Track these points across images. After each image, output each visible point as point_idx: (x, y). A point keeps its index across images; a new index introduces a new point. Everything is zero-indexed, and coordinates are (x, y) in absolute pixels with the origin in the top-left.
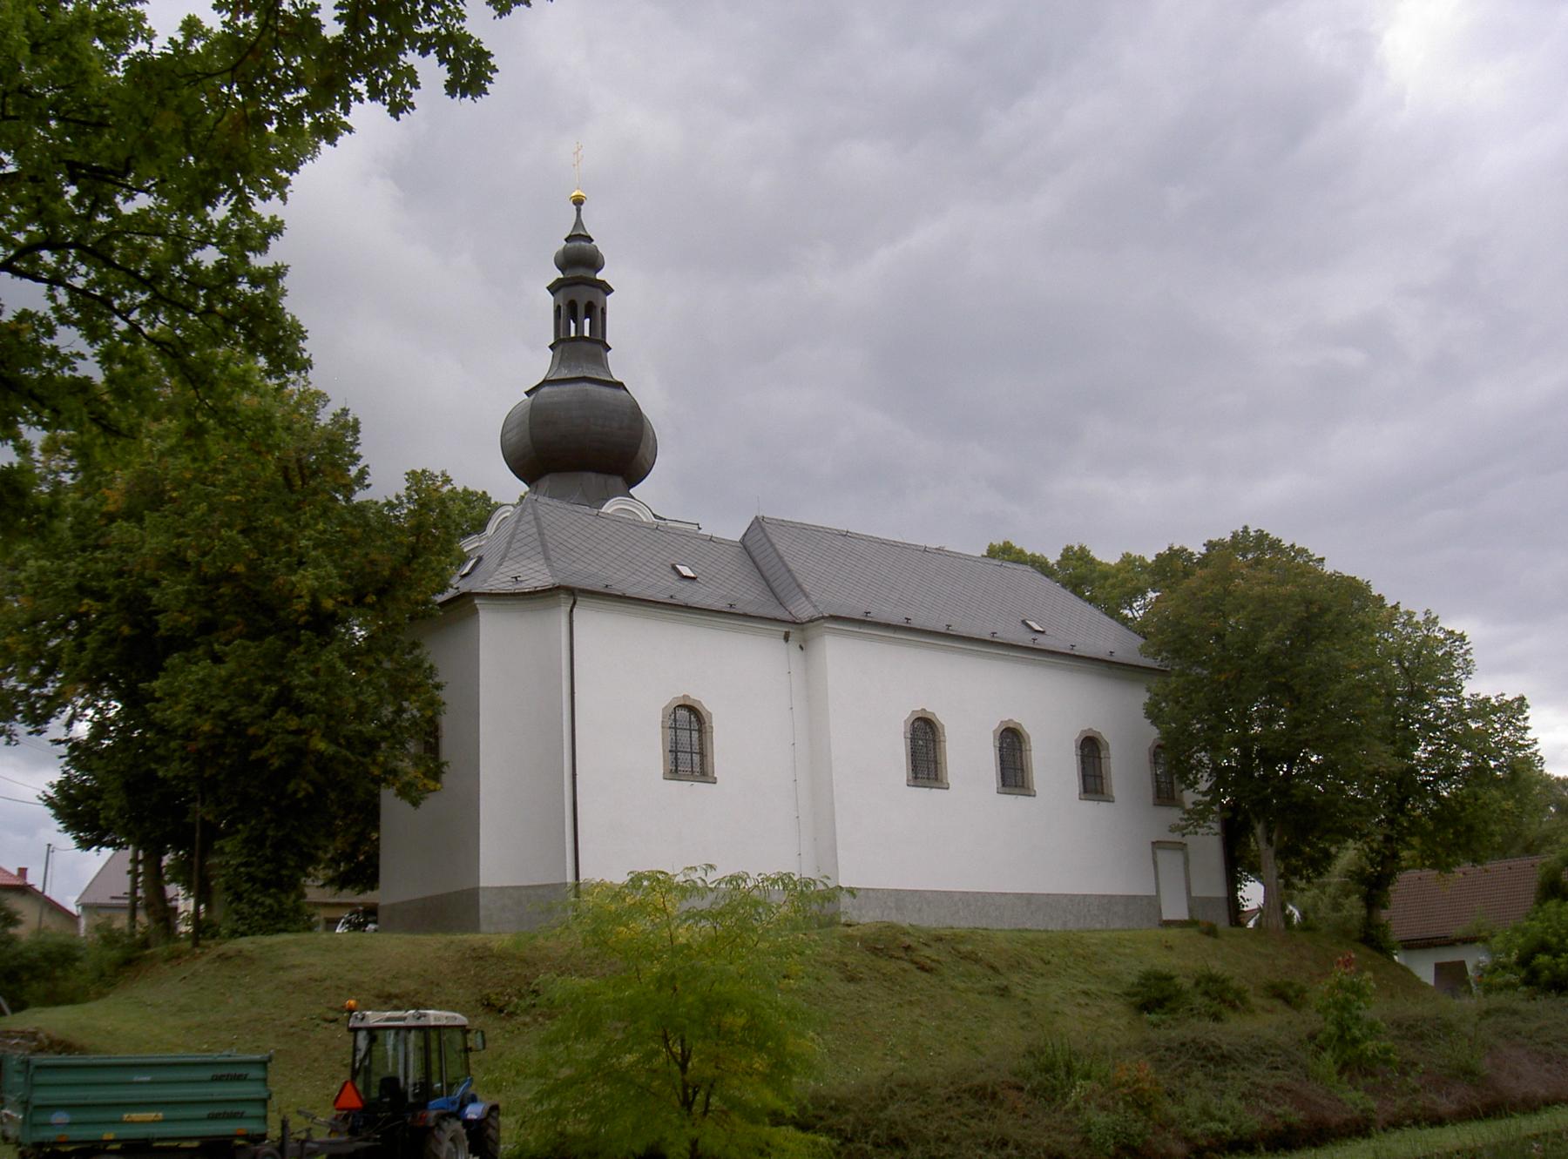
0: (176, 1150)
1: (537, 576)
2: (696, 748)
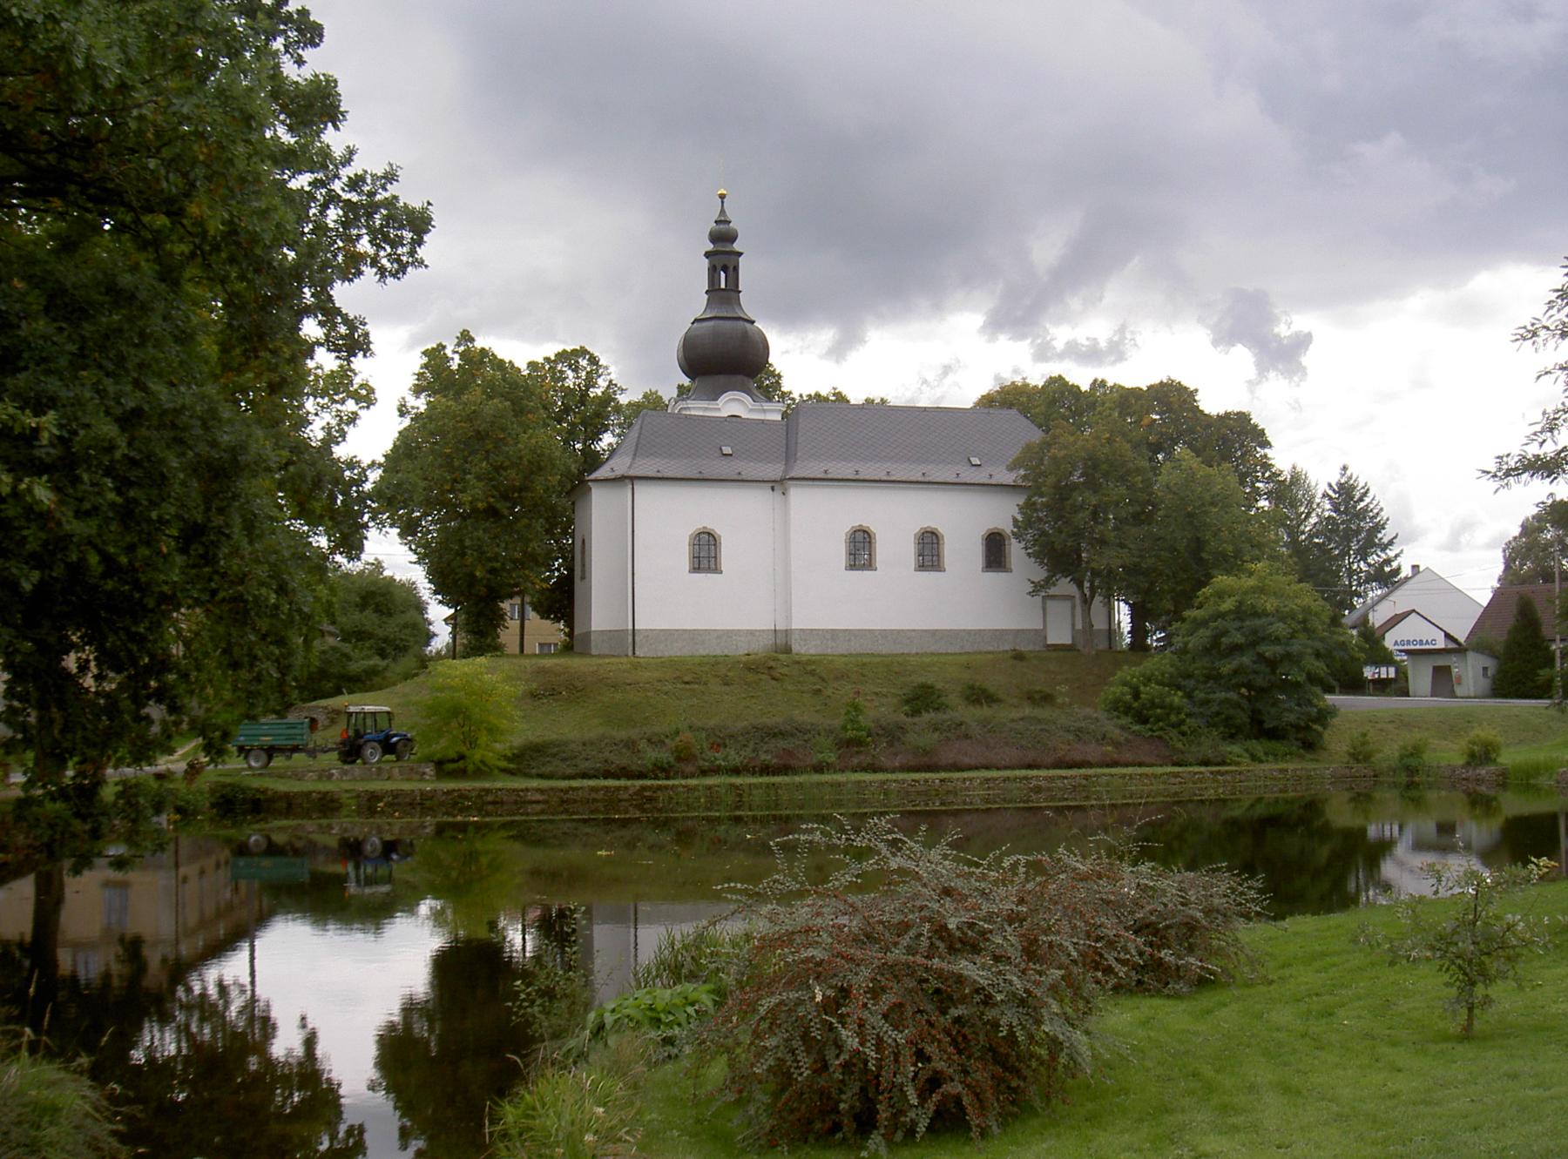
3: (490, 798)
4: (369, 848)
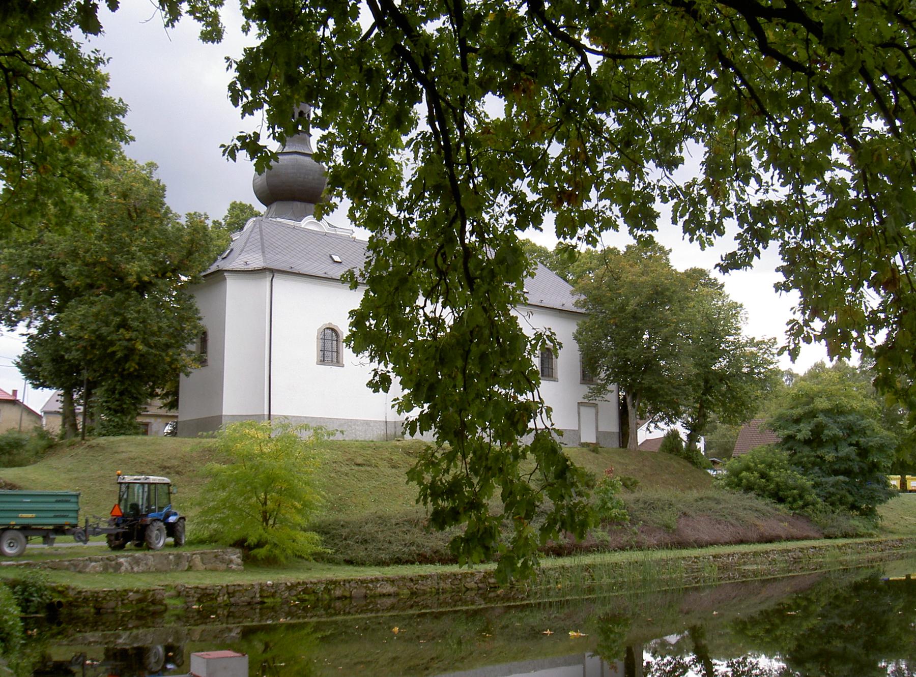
0: (41, 529)
1: (256, 262)
2: (335, 349)
3: (338, 593)
4: (153, 660)
